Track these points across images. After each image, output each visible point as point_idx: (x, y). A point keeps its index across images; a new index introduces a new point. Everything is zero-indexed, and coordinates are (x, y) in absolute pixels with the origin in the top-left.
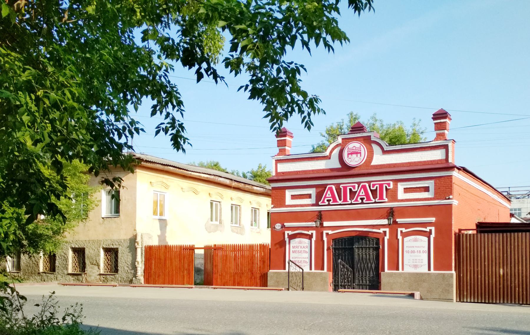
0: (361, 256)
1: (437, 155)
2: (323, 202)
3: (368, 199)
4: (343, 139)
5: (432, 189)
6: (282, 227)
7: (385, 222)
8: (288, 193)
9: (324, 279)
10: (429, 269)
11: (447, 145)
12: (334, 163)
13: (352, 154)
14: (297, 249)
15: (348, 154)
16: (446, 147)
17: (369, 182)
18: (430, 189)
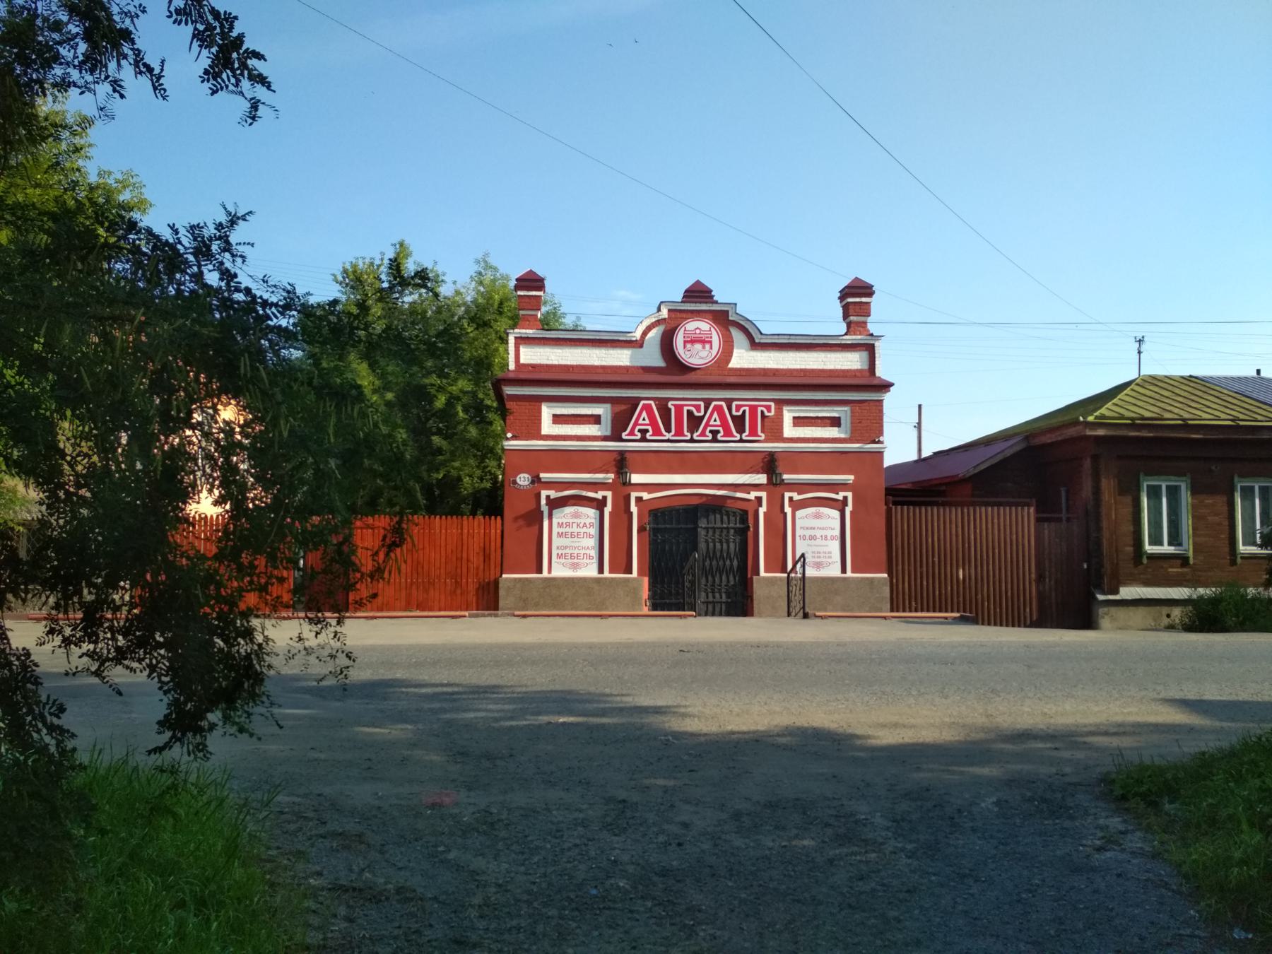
0: (711, 545)
1: (852, 361)
2: (632, 433)
3: (728, 433)
4: (669, 311)
5: (846, 421)
6: (533, 482)
7: (762, 479)
8: (547, 412)
9: (635, 592)
10: (844, 570)
11: (873, 345)
12: (651, 356)
13: (693, 342)
14: (567, 530)
15: (685, 342)
16: (870, 349)
17: (729, 402)
18: (843, 422)
